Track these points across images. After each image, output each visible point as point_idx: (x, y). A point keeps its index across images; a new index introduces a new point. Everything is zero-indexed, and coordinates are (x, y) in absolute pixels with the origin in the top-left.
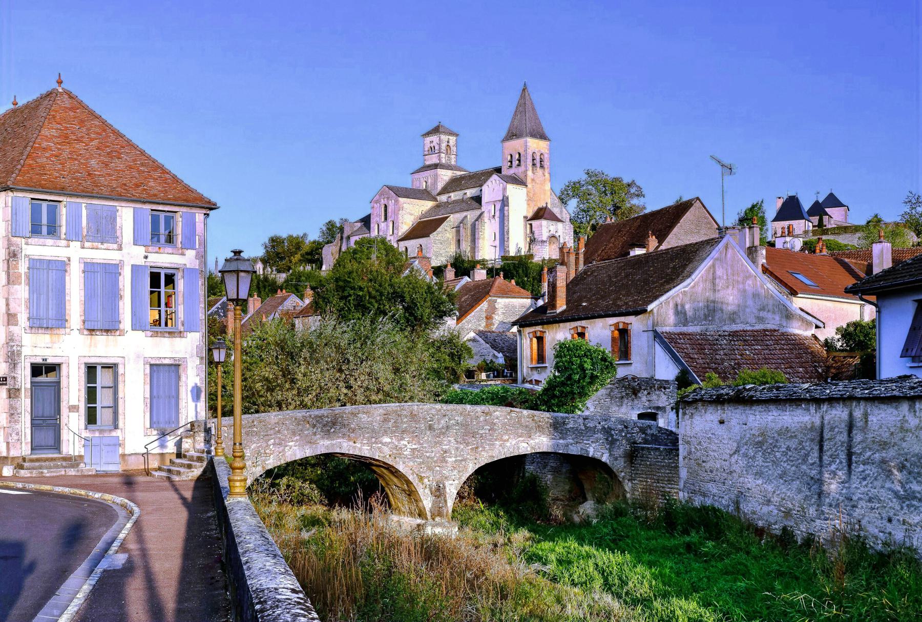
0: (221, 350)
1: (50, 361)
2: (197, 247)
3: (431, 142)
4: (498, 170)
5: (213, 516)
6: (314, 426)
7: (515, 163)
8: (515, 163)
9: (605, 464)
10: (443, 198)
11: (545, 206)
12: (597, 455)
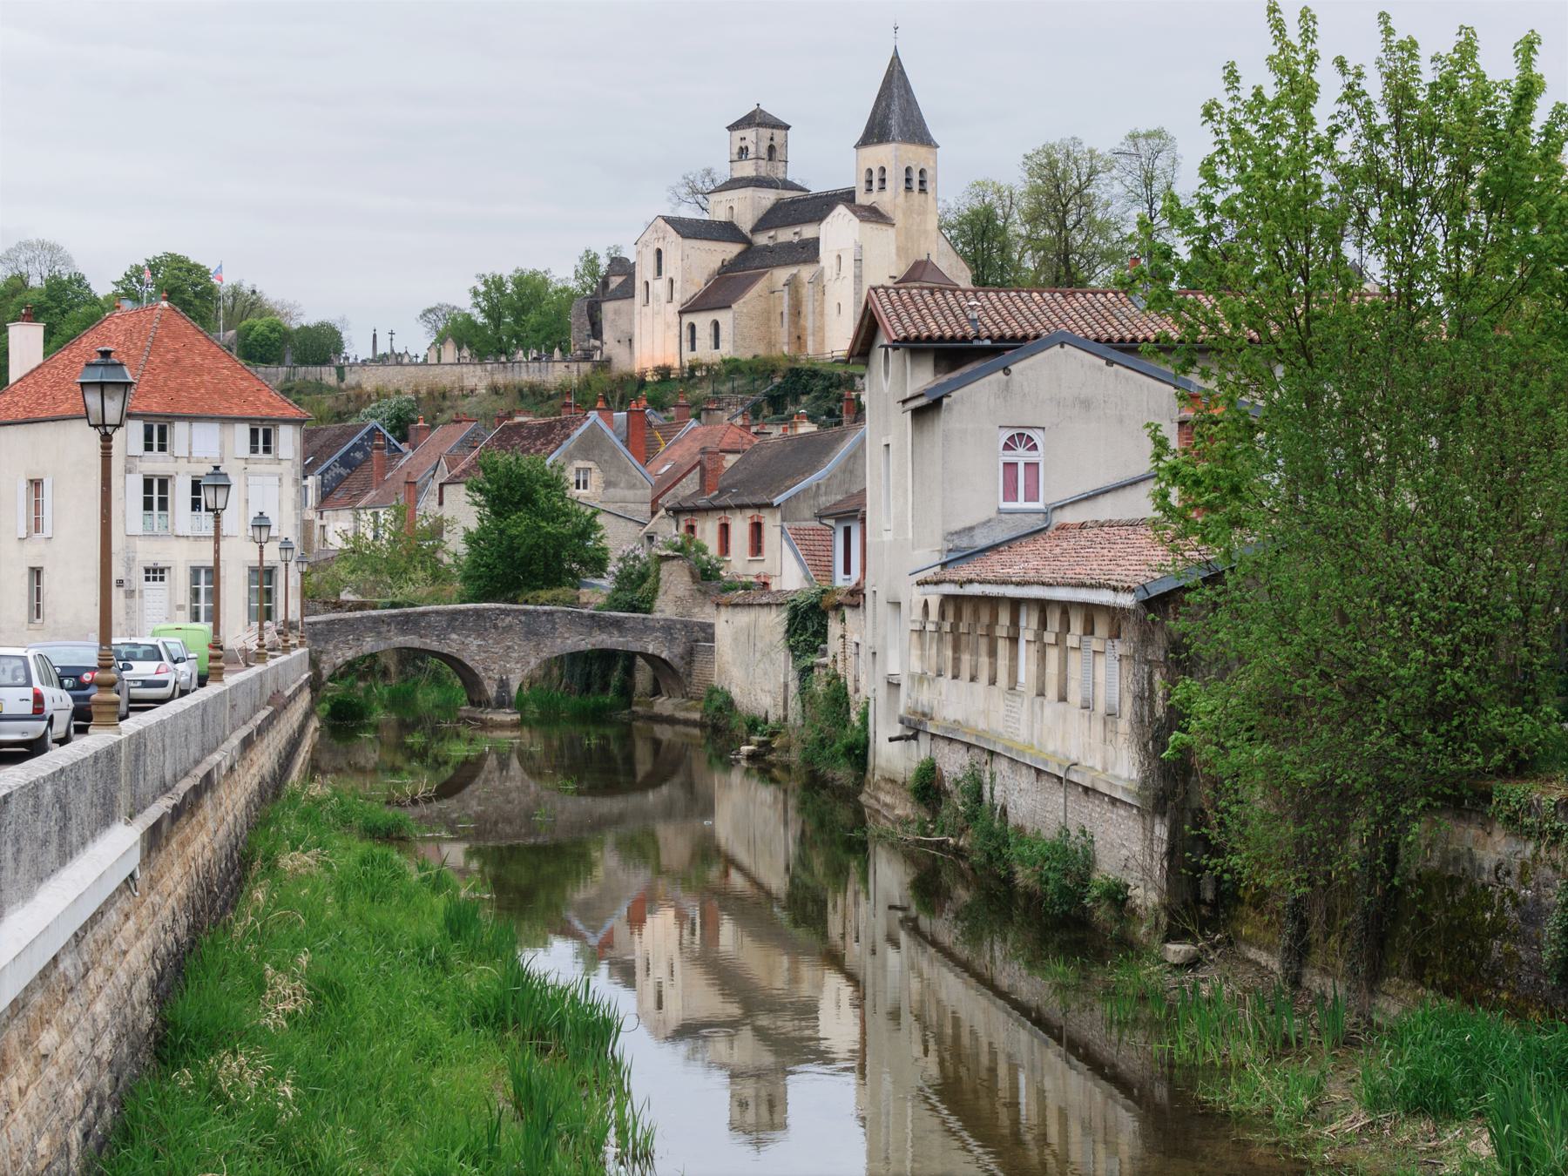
0: (388, 352)
1: (161, 565)
2: (306, 620)
3: (743, 139)
6: (389, 624)
7: (876, 184)
8: (876, 184)
9: (664, 661)
10: (762, 239)
11: (925, 258)
12: (657, 652)
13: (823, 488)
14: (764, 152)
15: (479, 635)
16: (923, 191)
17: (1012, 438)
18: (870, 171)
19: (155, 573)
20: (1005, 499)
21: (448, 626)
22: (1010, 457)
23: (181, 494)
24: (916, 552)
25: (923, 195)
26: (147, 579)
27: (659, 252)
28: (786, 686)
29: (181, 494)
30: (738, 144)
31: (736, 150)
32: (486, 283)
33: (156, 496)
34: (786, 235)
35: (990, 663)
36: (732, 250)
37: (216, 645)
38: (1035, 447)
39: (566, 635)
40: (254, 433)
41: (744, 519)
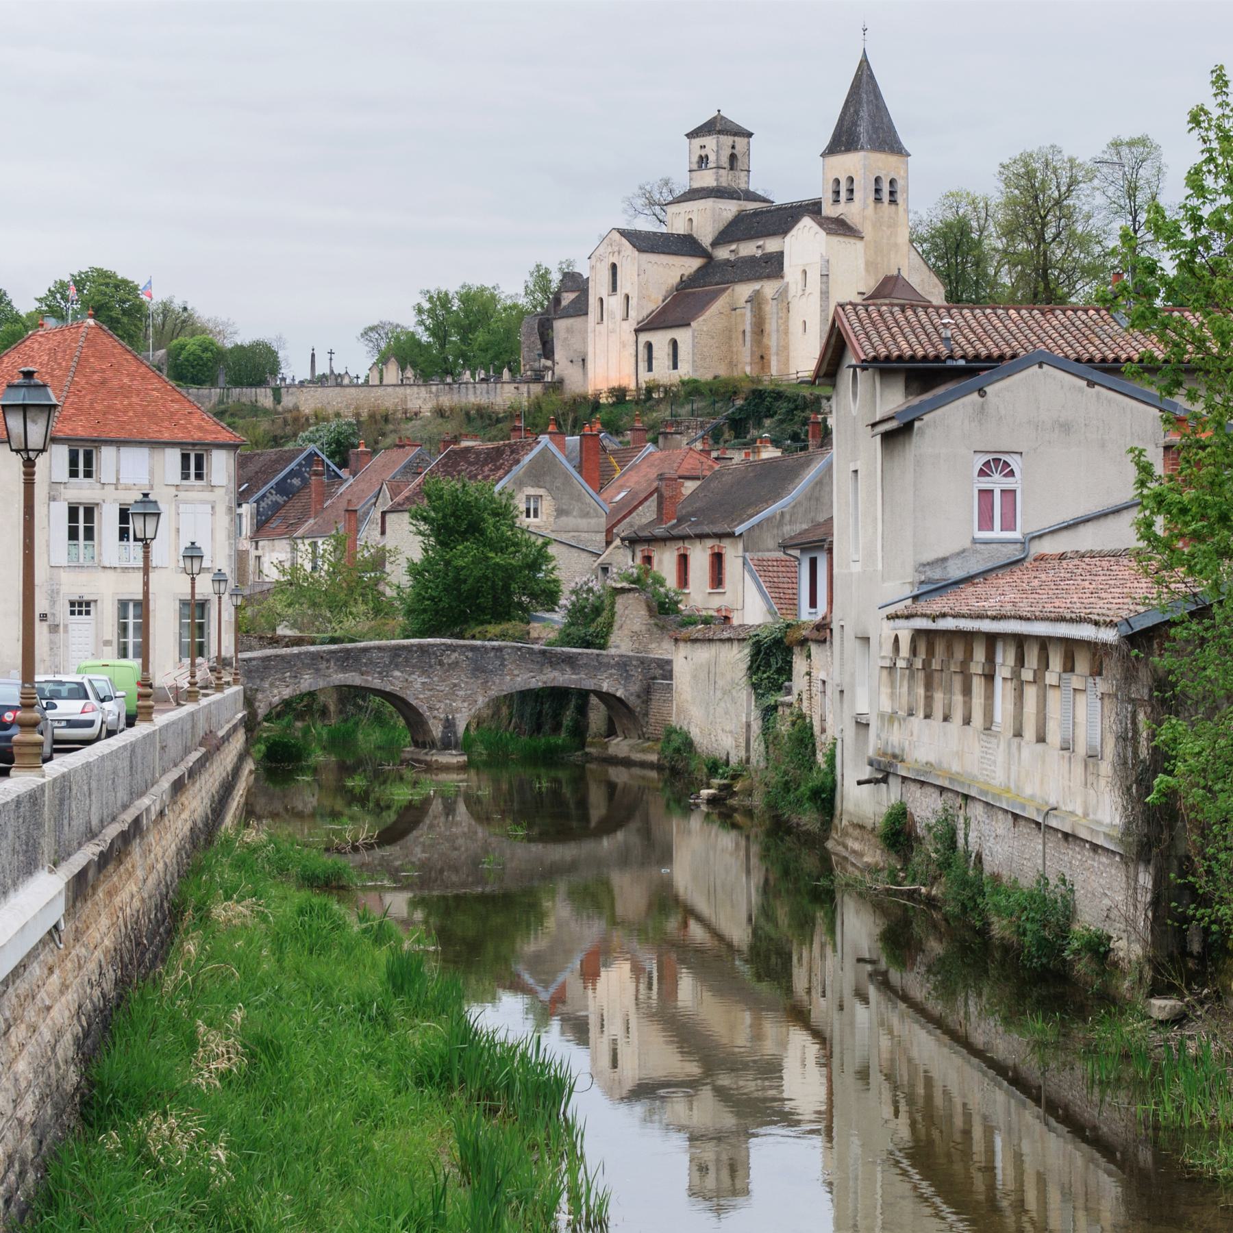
1: (86, 598)
3: (703, 147)
4: (813, 209)
5: (309, 829)
9: (619, 699)
11: (896, 273)
12: (611, 690)
13: (787, 517)
14: (725, 161)
15: (424, 672)
16: (893, 202)
17: (987, 464)
18: (837, 181)
19: (81, 607)
20: (980, 529)
21: (391, 663)
22: (985, 483)
23: (108, 522)
24: (885, 585)
25: (893, 207)
26: (72, 613)
27: (614, 266)
28: (748, 726)
29: (108, 522)
30: (698, 152)
31: (695, 159)
32: (431, 299)
33: (81, 525)
34: (748, 249)
35: (965, 702)
36: (692, 264)
37: (145, 683)
38: (1012, 473)
39: (516, 672)
40: (185, 458)
41: (704, 550)
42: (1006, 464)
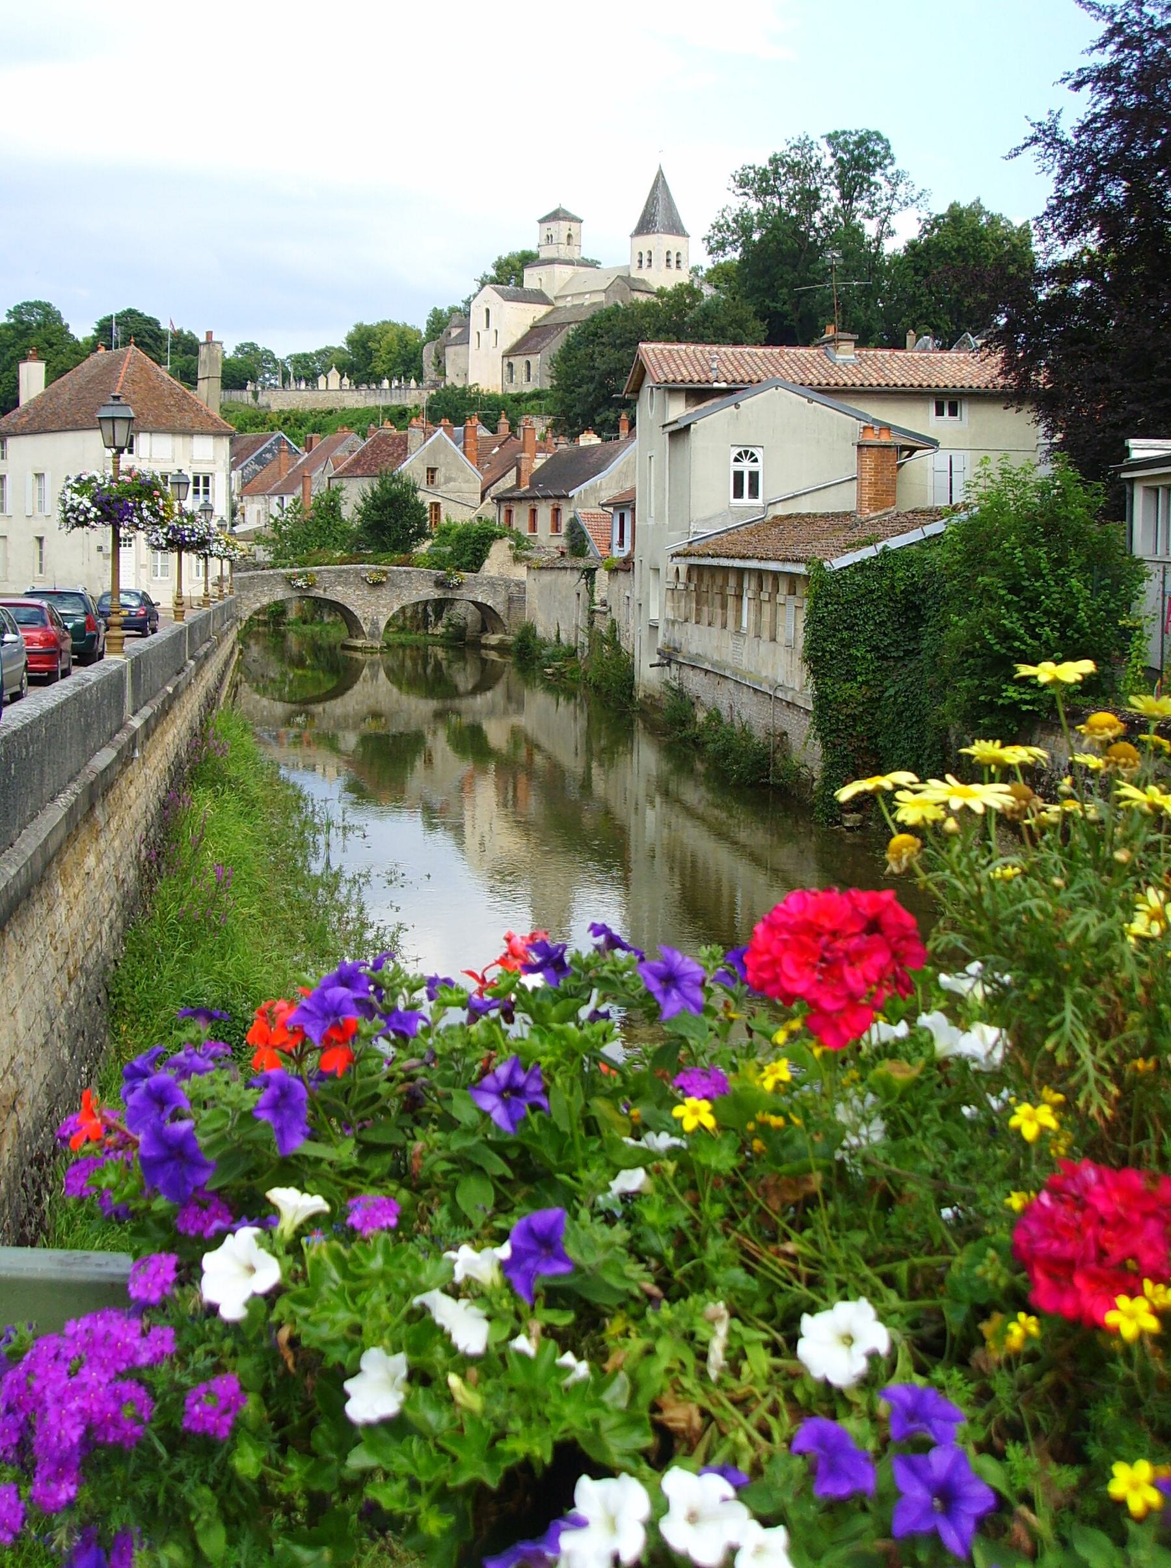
7: (645, 263)
8: (645, 263)
16: (678, 267)
17: (740, 454)
27: (488, 311)
38: (756, 461)
42: (752, 455)
